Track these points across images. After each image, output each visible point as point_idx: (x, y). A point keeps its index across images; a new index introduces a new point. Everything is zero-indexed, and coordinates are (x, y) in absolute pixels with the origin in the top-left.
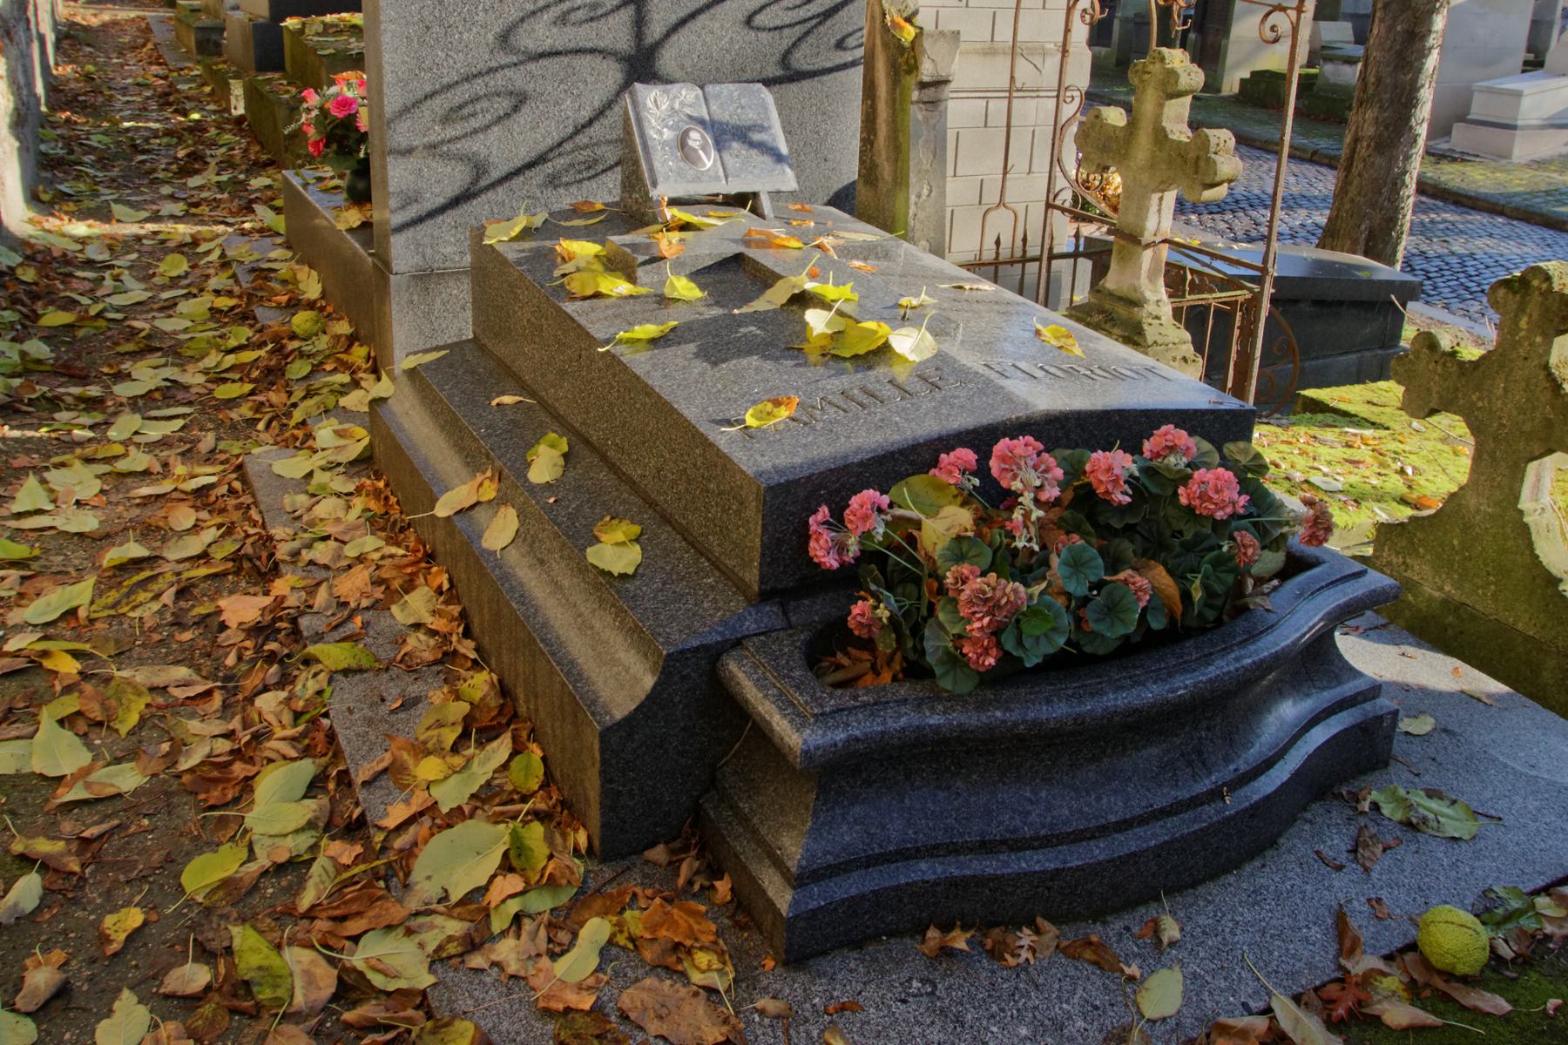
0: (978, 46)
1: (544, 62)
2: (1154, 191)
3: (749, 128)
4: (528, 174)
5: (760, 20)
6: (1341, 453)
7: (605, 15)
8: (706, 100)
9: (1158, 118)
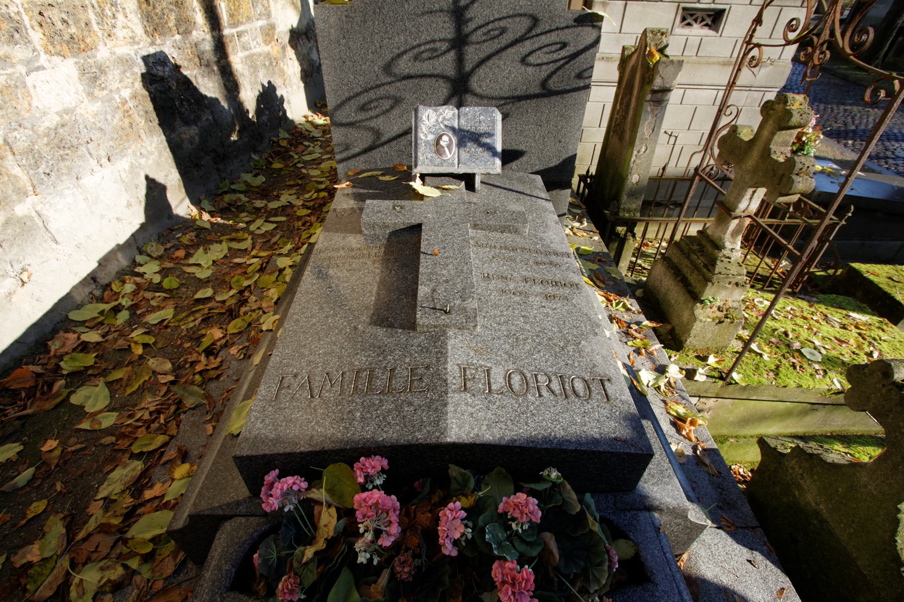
0: (721, 60)
1: (404, 82)
2: (750, 187)
3: (481, 135)
4: (399, 140)
5: (531, 59)
6: (837, 331)
8: (459, 116)
9: (769, 141)
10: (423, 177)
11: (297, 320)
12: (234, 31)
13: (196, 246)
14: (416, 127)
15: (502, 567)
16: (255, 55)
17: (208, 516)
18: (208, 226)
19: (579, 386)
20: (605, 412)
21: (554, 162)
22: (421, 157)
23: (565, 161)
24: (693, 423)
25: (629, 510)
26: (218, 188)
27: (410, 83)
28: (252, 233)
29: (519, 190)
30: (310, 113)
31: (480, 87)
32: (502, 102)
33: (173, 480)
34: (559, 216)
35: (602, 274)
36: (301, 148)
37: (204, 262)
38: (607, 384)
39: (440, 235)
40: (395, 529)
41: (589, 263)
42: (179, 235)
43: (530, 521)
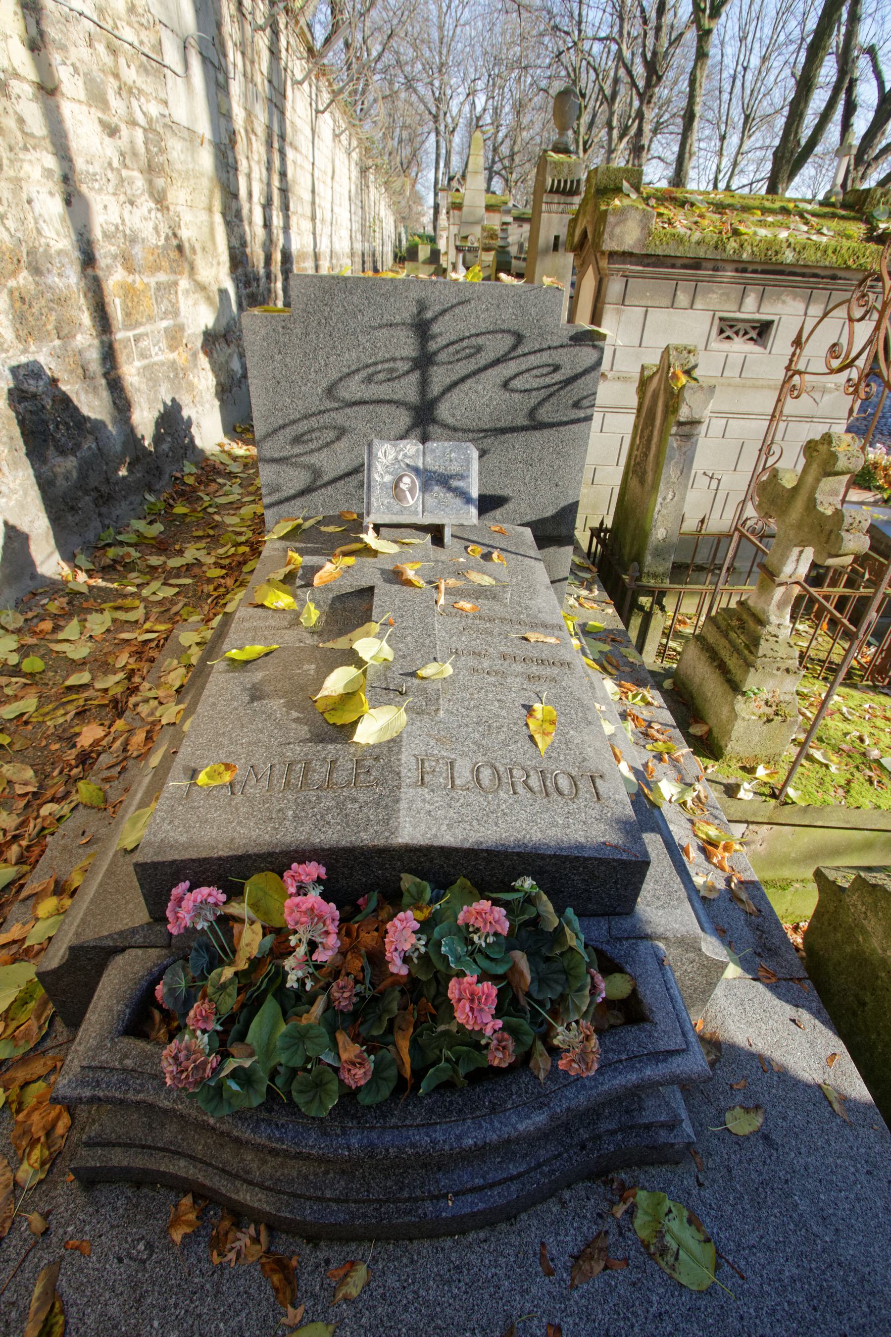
1: (356, 408)
3: (451, 477)
5: (516, 384)
7: (399, 377)
9: (814, 489)
10: (377, 528)
11: (214, 704)
12: (131, 334)
13: (67, 615)
14: (369, 466)
15: (460, 984)
17: (95, 947)
18: (85, 590)
19: (564, 783)
20: (594, 813)
21: (550, 512)
22: (375, 503)
23: (564, 509)
24: (726, 848)
25: (627, 938)
26: (99, 539)
27: (363, 410)
28: (144, 600)
30: (226, 441)
31: (453, 416)
33: (37, 919)
35: (616, 658)
36: (213, 487)
37: (75, 641)
38: (598, 781)
39: (397, 602)
40: (333, 941)
42: (45, 601)
43: (496, 934)
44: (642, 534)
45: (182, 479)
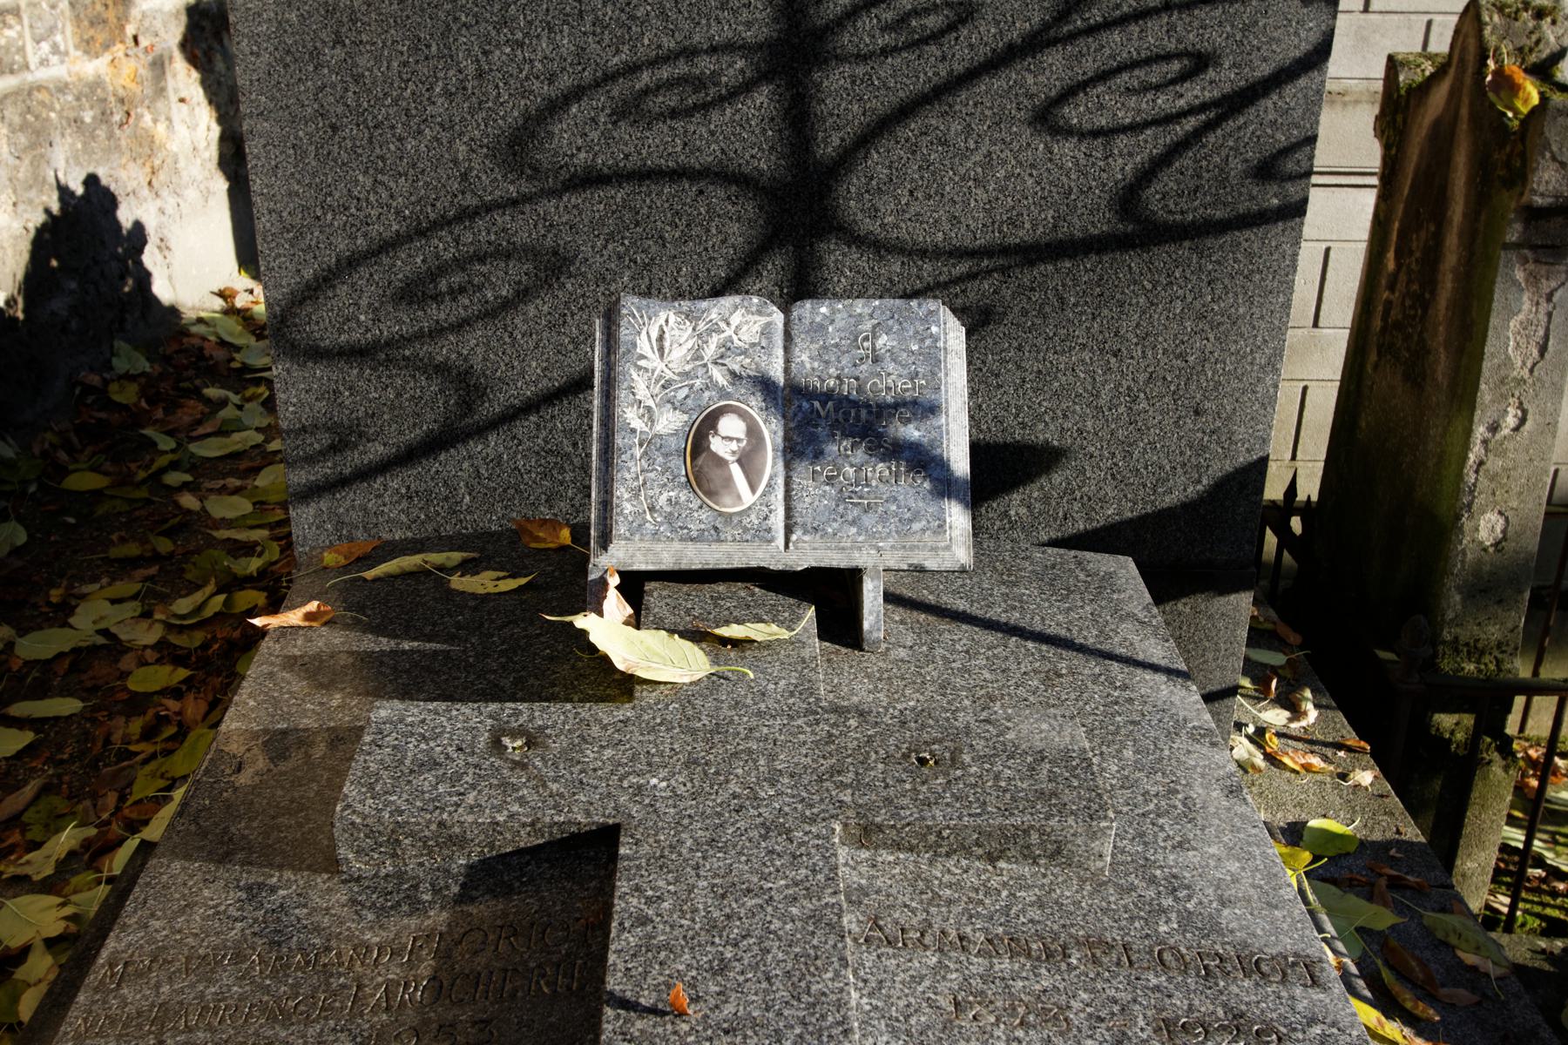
5: (1073, 114)
10: (634, 585)
14: (610, 383)
16: (39, 88)
21: (1179, 491)
27: (595, 203)
29: (1053, 630)
31: (874, 212)
32: (962, 268)
34: (1209, 698)
36: (190, 410)
39: (701, 899)
41: (1353, 901)
44: (1430, 522)
45: (102, 392)
